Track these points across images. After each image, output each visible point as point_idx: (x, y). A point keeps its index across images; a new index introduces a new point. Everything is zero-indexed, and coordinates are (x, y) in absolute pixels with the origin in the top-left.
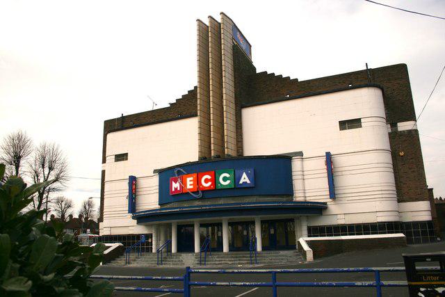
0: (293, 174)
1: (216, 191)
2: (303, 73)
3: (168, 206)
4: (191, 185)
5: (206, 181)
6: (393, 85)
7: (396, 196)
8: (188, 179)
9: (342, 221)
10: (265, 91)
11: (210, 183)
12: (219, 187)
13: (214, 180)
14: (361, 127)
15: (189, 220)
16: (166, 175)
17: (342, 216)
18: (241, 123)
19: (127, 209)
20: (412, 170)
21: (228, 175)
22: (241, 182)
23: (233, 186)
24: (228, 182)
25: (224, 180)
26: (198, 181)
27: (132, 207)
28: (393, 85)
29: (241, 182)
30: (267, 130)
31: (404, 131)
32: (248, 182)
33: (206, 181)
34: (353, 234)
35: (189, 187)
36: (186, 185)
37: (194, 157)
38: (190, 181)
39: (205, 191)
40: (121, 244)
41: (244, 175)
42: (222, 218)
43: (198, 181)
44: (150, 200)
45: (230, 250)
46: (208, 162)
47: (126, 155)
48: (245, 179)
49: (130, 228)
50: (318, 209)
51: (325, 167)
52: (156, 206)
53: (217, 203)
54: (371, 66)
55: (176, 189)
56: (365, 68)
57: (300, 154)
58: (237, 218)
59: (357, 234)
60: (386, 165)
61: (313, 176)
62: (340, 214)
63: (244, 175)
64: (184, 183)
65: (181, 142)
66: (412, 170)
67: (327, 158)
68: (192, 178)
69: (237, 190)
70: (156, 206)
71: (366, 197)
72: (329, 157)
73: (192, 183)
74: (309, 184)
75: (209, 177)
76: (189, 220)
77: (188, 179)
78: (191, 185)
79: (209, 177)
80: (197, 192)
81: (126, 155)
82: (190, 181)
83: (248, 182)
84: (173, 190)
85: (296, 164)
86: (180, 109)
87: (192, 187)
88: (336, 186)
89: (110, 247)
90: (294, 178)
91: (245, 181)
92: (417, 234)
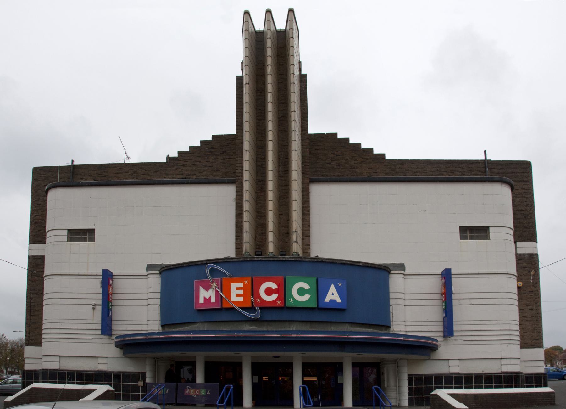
0: (391, 296)
1: (284, 310)
2: (394, 146)
3: (188, 328)
4: (238, 296)
5: (269, 292)
6: (516, 176)
7: (518, 338)
8: (234, 286)
9: (455, 369)
10: (333, 163)
11: (274, 297)
12: (290, 303)
13: (283, 290)
14: (461, 239)
15: (284, 355)
16: (177, 278)
17: (457, 363)
18: (309, 206)
19: (99, 327)
20: (530, 307)
21: (306, 286)
22: (327, 300)
23: (314, 305)
24: (307, 297)
25: (300, 292)
26: (253, 290)
27: (107, 327)
28: (516, 176)
29: (327, 300)
30: (344, 224)
31: (524, 254)
32: (339, 300)
33: (269, 292)
34: (511, 387)
35: (234, 298)
36: (229, 296)
37: (226, 249)
38: (238, 289)
39: (266, 308)
40: (112, 389)
41: (333, 289)
42: (242, 354)
43: (253, 290)
44: (142, 315)
45: (355, 404)
46: (249, 261)
47: (91, 232)
48: (333, 295)
49: (100, 360)
50: (423, 348)
51: (100, 290)
52: (156, 327)
53: (283, 329)
54: (492, 157)
55: (207, 300)
56: (483, 158)
57: (401, 267)
58: (267, 355)
59: (536, 386)
60: (432, 296)
61: (413, 303)
62: (454, 357)
63: (333, 289)
64: (224, 289)
65: (205, 224)
66: (530, 307)
67: (103, 278)
68: (241, 285)
69: (319, 311)
70: (156, 327)
71: (485, 341)
72: (107, 277)
73: (241, 292)
74: (411, 313)
75: (274, 286)
76: (284, 355)
77: (234, 286)
78: (238, 296)
79: (274, 286)
80: (251, 309)
81: (91, 232)
82: (238, 289)
83: (339, 300)
84: (201, 301)
85: (396, 283)
86: (206, 163)
87: (241, 299)
88: (113, 318)
89: (451, 395)
90: (392, 302)
91: (333, 298)
92: (126, 388)
